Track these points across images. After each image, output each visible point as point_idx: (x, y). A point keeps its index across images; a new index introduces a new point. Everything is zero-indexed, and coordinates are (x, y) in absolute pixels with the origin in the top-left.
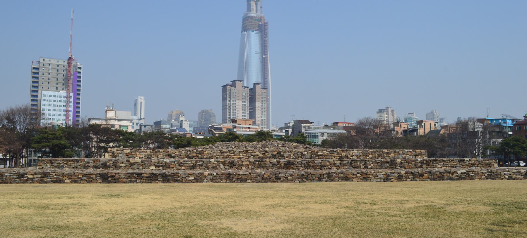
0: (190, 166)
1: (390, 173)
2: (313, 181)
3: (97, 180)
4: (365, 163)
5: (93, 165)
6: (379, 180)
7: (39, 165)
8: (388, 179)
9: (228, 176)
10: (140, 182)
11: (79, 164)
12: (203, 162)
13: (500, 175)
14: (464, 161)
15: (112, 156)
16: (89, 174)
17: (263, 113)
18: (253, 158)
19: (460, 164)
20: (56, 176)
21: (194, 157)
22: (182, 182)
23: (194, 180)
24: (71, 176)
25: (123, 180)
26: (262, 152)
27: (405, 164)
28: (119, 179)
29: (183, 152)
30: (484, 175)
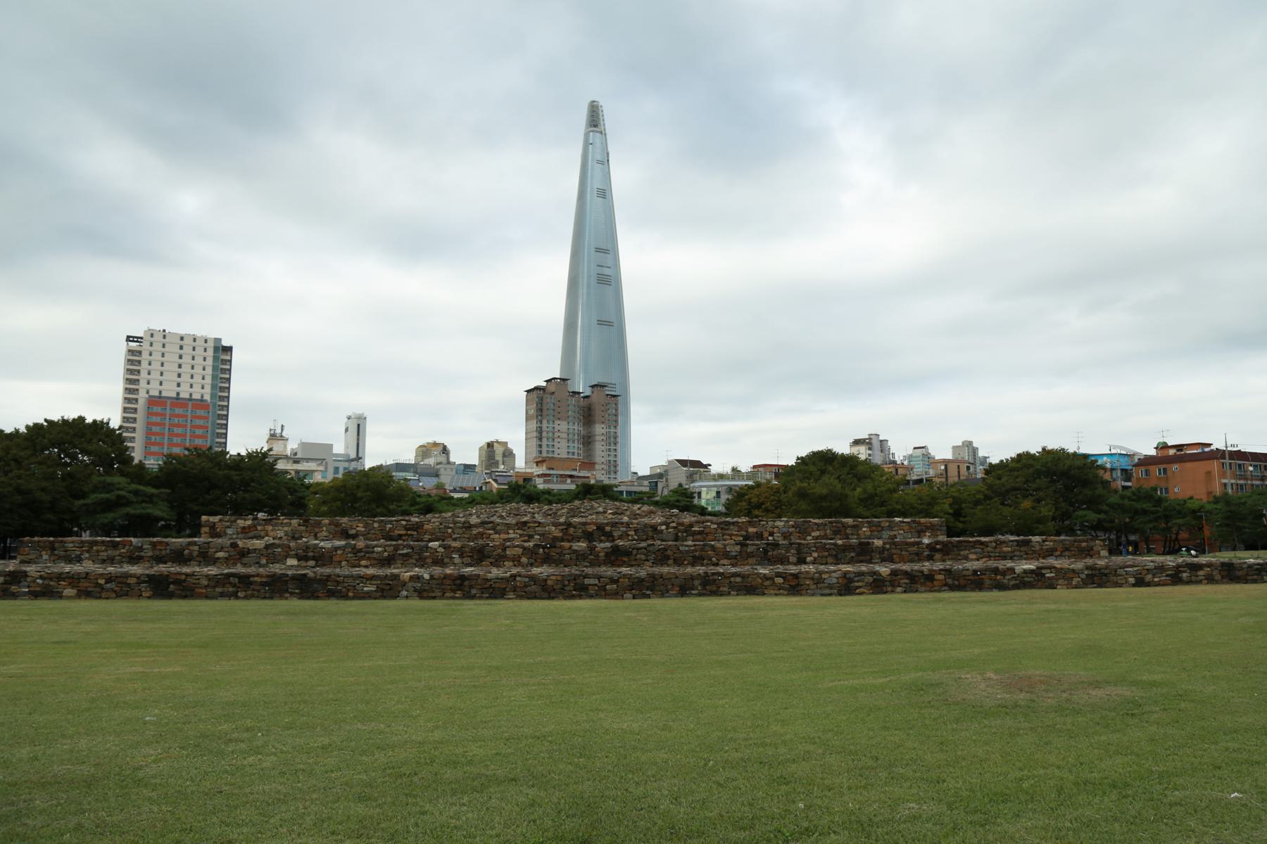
0: (381, 558)
1: (854, 575)
2: (667, 595)
3: (140, 590)
4: (799, 551)
5: (150, 554)
6: (827, 591)
7: (21, 553)
8: (849, 587)
9: (458, 582)
10: (246, 598)
11: (118, 553)
12: (413, 548)
13: (1116, 575)
14: (1031, 544)
15: (209, 533)
16: (123, 575)
17: (612, 447)
18: (540, 539)
19: (1021, 551)
20: (39, 581)
21: (400, 536)
22: (346, 597)
23: (375, 591)
24: (77, 581)
25: (204, 591)
26: (560, 525)
27: (894, 551)
28: (195, 588)
29: (376, 525)
30: (1077, 575)
